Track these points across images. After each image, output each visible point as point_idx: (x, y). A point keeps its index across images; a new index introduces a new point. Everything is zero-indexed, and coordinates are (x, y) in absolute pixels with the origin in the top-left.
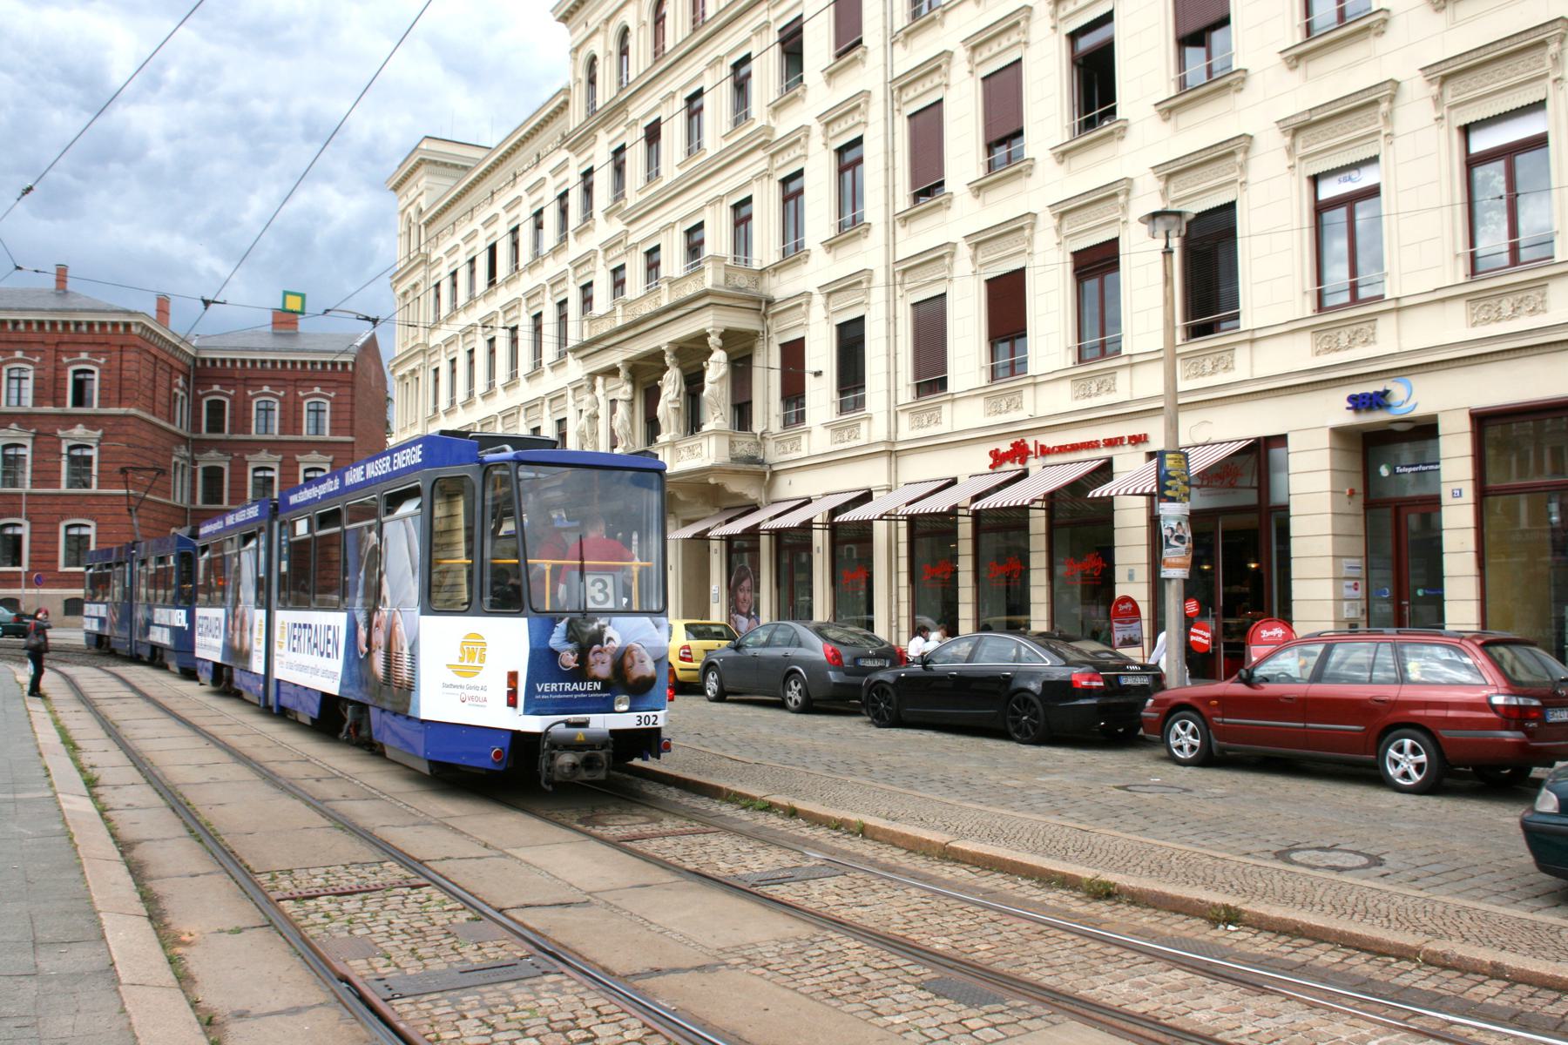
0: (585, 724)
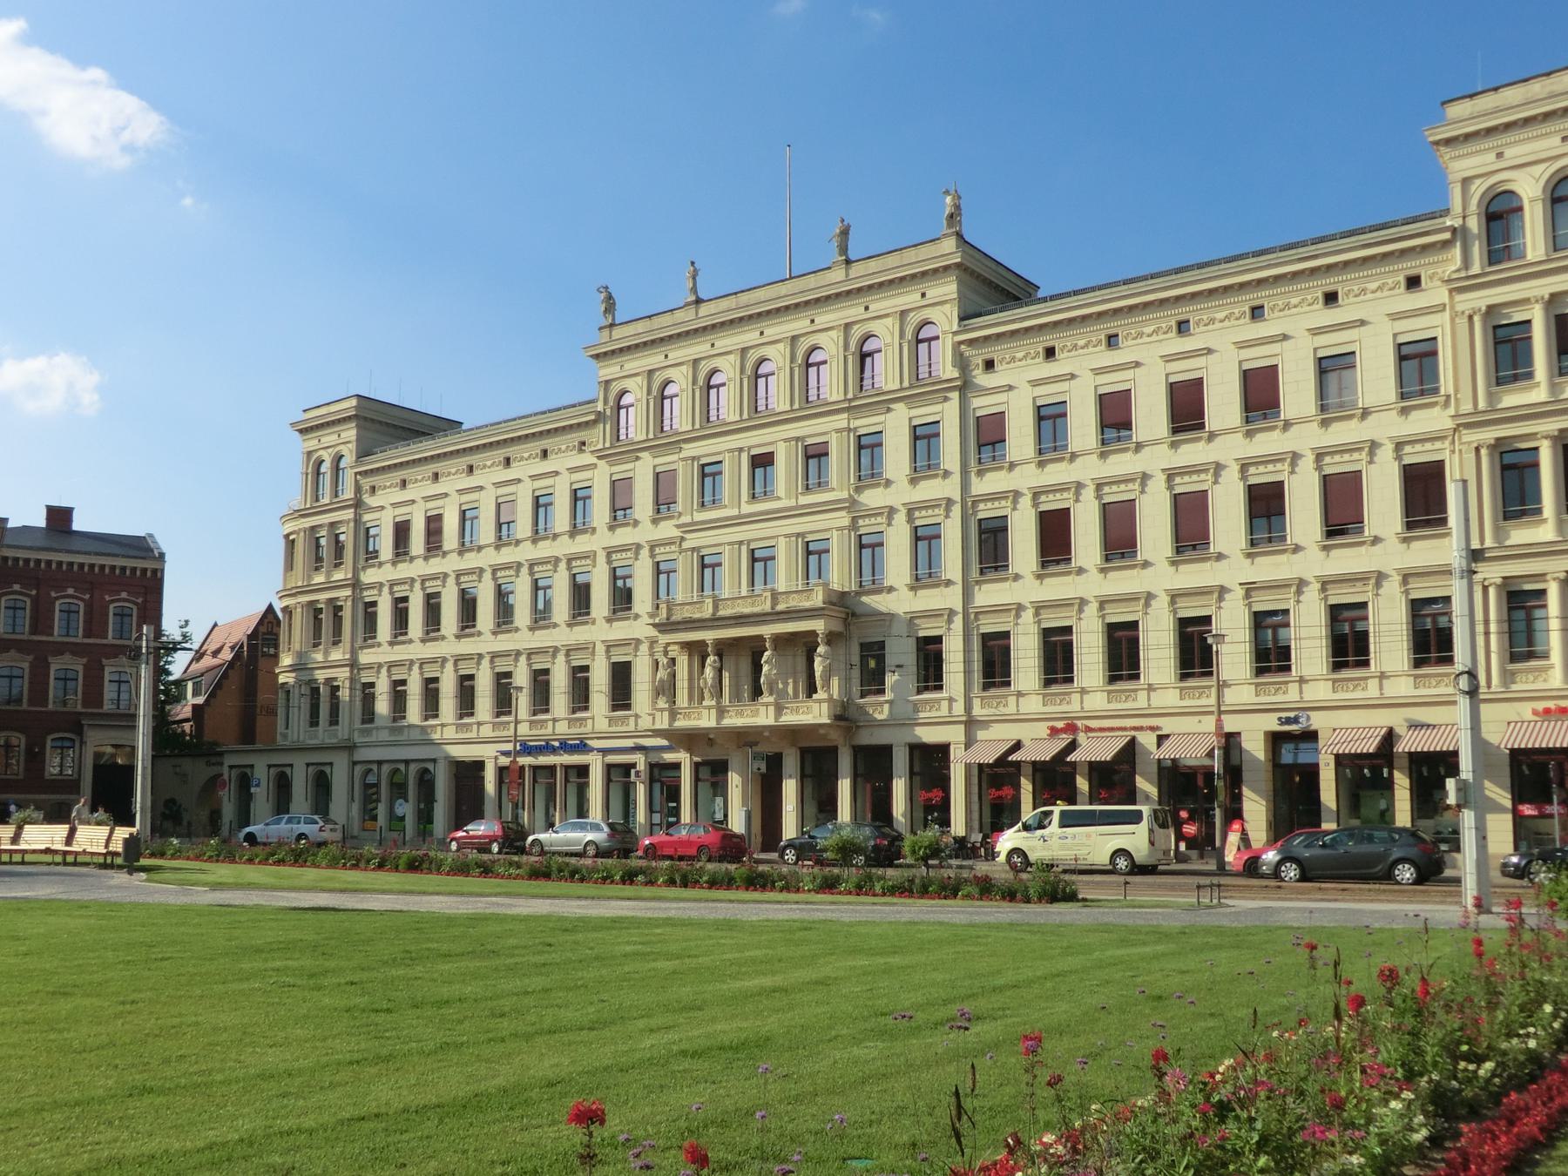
0: (971, 868)
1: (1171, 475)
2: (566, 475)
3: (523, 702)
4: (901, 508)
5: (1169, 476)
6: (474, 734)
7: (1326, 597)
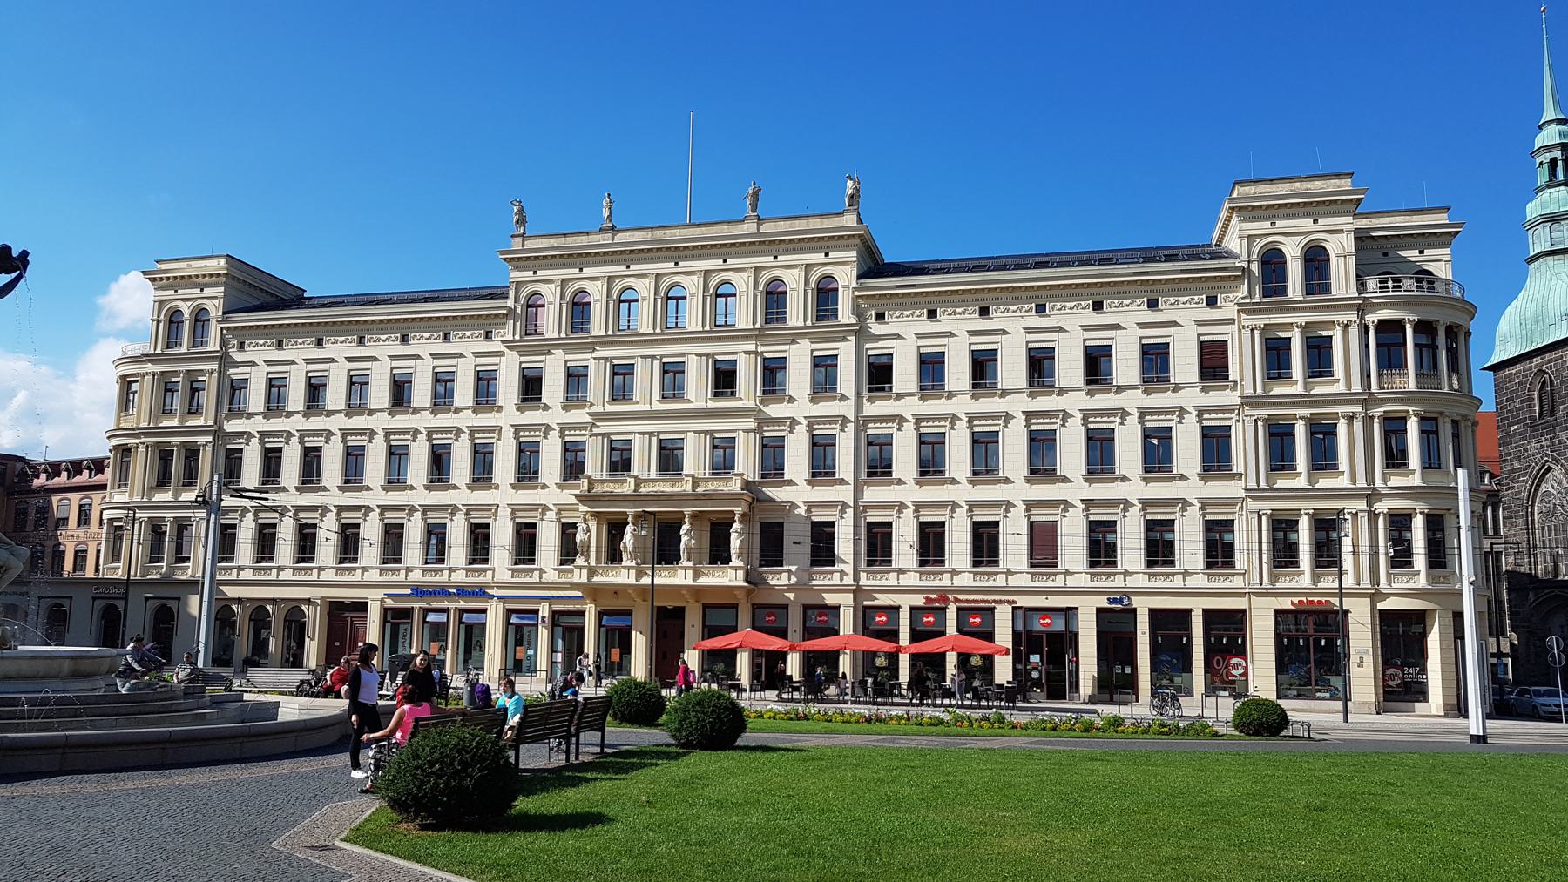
1: (1087, 415)
2: (303, 367)
3: (285, 550)
4: (296, 433)
5: (429, 432)
6: (314, 577)
7: (426, 519)
